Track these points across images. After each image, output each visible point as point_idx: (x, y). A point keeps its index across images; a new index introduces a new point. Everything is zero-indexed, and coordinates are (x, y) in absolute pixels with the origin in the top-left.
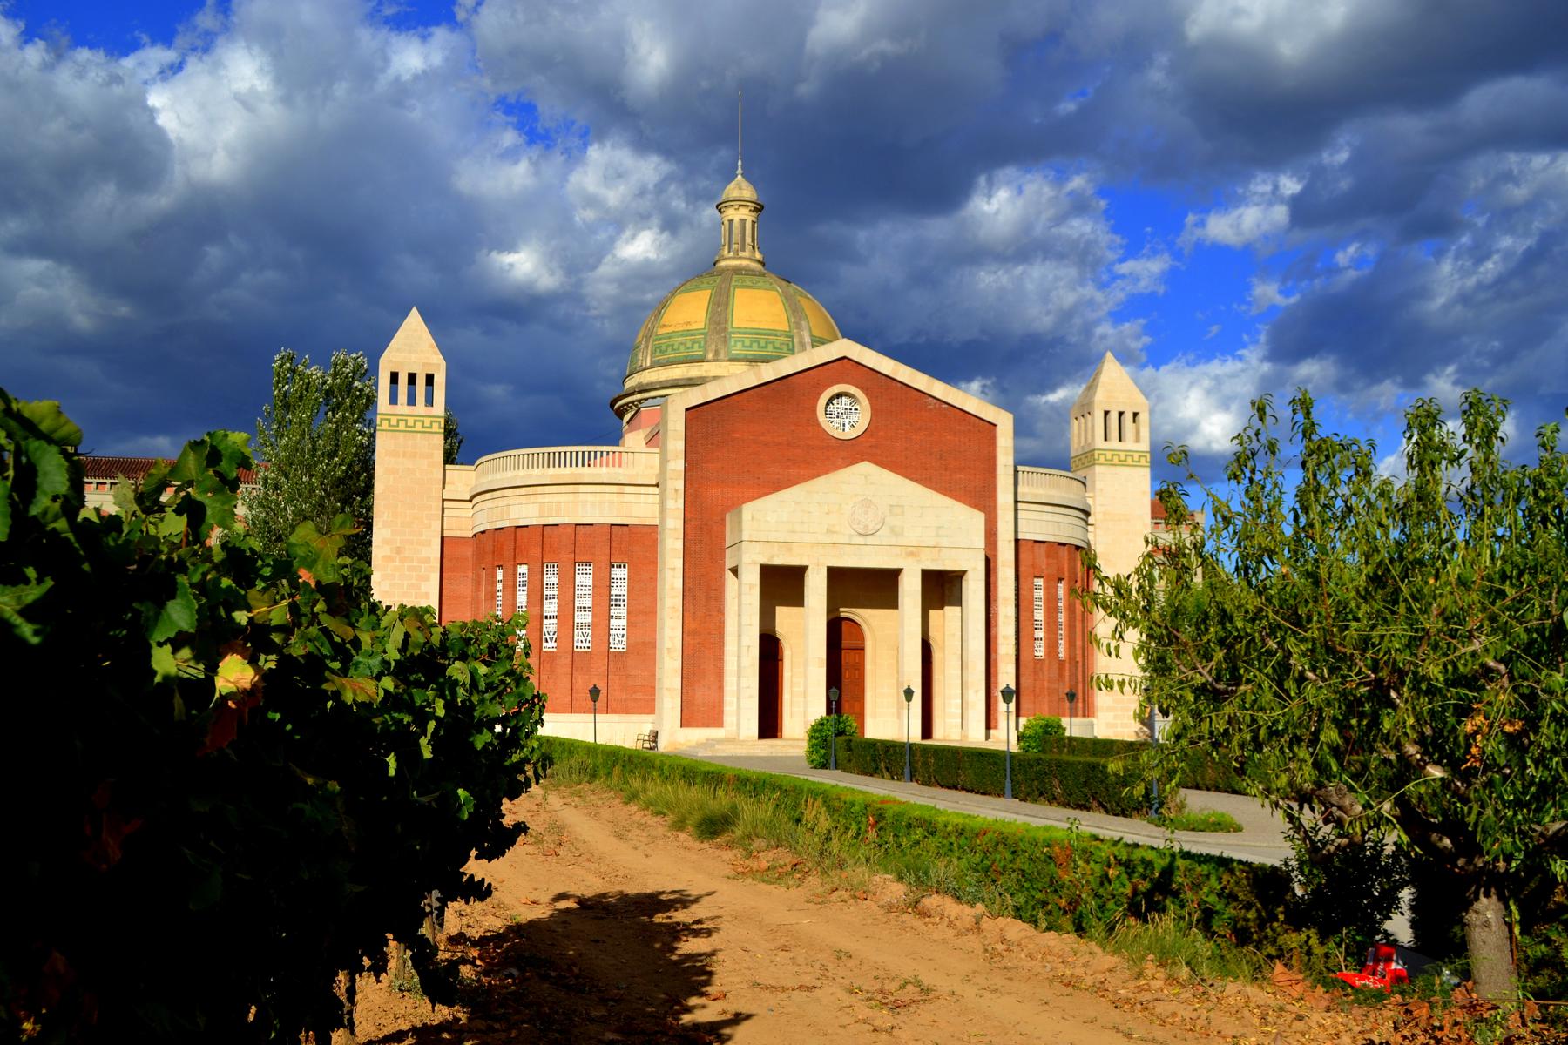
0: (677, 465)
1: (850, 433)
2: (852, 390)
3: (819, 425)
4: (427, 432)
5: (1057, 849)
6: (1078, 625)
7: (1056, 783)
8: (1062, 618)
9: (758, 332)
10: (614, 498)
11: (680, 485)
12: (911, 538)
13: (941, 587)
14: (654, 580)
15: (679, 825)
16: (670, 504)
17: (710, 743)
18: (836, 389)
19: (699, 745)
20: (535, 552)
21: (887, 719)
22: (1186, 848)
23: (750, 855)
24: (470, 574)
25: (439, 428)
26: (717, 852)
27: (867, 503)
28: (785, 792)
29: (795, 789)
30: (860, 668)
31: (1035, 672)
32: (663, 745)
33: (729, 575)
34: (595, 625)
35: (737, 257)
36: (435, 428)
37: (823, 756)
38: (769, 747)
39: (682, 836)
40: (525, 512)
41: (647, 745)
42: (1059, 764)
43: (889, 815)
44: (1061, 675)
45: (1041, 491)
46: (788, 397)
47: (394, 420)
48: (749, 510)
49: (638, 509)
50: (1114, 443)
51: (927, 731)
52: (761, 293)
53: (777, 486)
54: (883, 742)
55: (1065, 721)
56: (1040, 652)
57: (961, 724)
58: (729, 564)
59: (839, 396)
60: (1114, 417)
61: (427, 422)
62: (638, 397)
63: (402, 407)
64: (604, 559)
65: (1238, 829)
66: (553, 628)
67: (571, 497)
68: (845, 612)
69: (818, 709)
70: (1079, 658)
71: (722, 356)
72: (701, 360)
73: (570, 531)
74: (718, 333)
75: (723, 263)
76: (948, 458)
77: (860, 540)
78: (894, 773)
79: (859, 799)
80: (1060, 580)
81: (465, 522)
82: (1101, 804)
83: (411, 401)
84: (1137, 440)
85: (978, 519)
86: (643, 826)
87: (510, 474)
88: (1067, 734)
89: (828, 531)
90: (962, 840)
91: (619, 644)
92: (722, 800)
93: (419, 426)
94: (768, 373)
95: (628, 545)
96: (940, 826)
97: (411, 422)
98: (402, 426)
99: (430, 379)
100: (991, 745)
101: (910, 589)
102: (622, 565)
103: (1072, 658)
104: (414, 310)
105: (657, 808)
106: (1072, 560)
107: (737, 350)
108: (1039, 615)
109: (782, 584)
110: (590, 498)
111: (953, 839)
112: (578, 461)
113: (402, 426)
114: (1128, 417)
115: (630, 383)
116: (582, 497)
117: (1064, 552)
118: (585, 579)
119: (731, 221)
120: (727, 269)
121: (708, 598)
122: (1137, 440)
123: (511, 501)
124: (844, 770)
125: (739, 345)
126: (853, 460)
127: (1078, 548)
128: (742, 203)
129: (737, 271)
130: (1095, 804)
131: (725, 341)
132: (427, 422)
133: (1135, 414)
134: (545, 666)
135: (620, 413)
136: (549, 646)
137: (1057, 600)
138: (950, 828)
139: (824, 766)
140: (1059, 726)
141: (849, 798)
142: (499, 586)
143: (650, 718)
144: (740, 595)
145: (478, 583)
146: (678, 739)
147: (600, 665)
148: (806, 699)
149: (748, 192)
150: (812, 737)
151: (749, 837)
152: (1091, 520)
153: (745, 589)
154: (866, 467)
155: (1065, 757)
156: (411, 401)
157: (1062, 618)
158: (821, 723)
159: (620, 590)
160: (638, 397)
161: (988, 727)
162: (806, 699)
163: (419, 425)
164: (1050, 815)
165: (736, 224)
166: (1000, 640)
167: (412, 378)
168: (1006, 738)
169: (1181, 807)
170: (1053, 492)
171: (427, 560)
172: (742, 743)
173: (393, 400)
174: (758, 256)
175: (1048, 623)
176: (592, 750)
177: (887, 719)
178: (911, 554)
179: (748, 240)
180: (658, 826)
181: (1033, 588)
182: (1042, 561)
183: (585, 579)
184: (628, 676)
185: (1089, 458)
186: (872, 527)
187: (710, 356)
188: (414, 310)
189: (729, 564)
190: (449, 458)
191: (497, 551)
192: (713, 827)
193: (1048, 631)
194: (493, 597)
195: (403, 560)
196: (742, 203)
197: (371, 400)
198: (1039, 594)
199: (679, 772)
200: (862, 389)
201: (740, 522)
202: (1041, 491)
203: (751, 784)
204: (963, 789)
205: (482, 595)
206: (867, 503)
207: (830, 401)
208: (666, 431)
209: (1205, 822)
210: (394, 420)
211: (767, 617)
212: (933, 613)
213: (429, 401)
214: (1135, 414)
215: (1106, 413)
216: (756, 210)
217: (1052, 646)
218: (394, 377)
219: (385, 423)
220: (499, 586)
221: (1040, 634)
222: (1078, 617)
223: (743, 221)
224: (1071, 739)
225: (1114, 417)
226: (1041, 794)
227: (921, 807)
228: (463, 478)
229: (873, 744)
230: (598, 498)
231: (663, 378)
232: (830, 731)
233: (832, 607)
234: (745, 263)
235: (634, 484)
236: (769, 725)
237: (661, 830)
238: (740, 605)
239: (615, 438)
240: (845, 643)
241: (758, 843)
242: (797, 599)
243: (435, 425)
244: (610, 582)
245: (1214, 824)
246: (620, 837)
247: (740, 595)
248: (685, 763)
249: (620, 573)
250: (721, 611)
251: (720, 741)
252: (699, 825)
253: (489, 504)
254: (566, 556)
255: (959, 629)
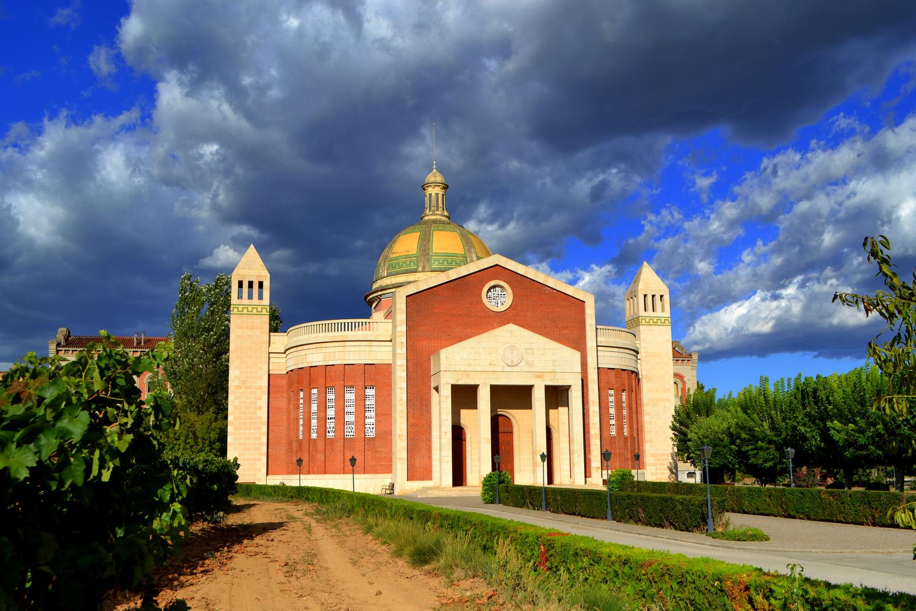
0: (402, 328)
1: (501, 308)
2: (502, 283)
3: (483, 304)
4: (259, 314)
5: (729, 583)
6: (634, 416)
7: (640, 510)
8: (625, 412)
9: (447, 255)
10: (367, 349)
11: (404, 340)
12: (538, 367)
13: (557, 396)
14: (390, 395)
15: (398, 554)
16: (399, 351)
17: (425, 490)
18: (492, 283)
19: (418, 491)
20: (322, 381)
21: (527, 473)
22: (806, 574)
23: (452, 584)
24: (285, 395)
25: (266, 312)
26: (427, 579)
27: (512, 348)
28: (475, 526)
29: (481, 523)
30: (510, 444)
31: (611, 444)
32: (397, 491)
33: (434, 391)
34: (356, 423)
35: (434, 214)
36: (264, 312)
37: (492, 496)
38: (458, 491)
39: (400, 562)
40: (315, 358)
41: (388, 492)
42: (642, 499)
43: (558, 545)
44: (626, 445)
45: (611, 340)
46: (466, 287)
47: (240, 308)
48: (444, 353)
49: (380, 355)
50: (650, 313)
51: (550, 480)
52: (448, 233)
53: (460, 339)
54: (528, 487)
55: (634, 472)
56: (613, 433)
57: (570, 476)
58: (433, 385)
59: (494, 287)
60: (649, 298)
61: (260, 308)
62: (380, 293)
63: (245, 301)
64: (361, 384)
65: (767, 539)
66: (332, 425)
67: (341, 349)
68: (501, 412)
69: (487, 469)
70: (635, 436)
71: (427, 269)
72: (415, 271)
73: (341, 368)
74: (424, 256)
75: (426, 218)
76: (556, 318)
77: (509, 369)
78: (536, 506)
79: (531, 531)
80: (624, 390)
81: (281, 365)
82: (671, 524)
83: (250, 297)
84: (663, 311)
85: (577, 355)
86: (374, 553)
87: (306, 337)
88: (635, 479)
89: (490, 364)
90: (626, 569)
91: (371, 433)
92: (429, 535)
93: (255, 311)
94: (453, 275)
95: (375, 375)
96: (605, 556)
97: (250, 309)
98: (245, 311)
99: (261, 285)
100: (588, 487)
101: (539, 397)
102: (372, 387)
103: (631, 435)
104: (252, 245)
105: (385, 538)
106: (630, 379)
107: (435, 265)
108: (612, 411)
109: (464, 396)
110: (352, 349)
111: (617, 567)
112: (345, 328)
113: (245, 311)
114: (658, 298)
115: (375, 286)
116: (348, 349)
117: (625, 374)
118: (350, 396)
119: (430, 195)
120: (429, 221)
121: (422, 405)
122: (663, 311)
123: (308, 352)
124: (505, 504)
125: (437, 263)
126: (503, 323)
127: (633, 372)
128: (436, 184)
129: (435, 222)
130: (667, 524)
131: (428, 260)
132: (260, 308)
133: (662, 296)
134: (328, 447)
135: (370, 303)
136: (331, 435)
137: (622, 402)
138: (613, 558)
139: (492, 502)
140: (631, 475)
141: (523, 531)
142: (301, 401)
143: (389, 475)
144: (440, 402)
145: (289, 400)
146: (406, 487)
147: (360, 446)
148: (479, 464)
149: (439, 179)
150: (484, 485)
151: (451, 567)
152: (639, 357)
153: (443, 399)
154: (511, 327)
155: (645, 494)
156: (250, 297)
157: (625, 412)
158: (490, 476)
159: (370, 402)
160: (380, 293)
161: (586, 477)
162: (479, 464)
163: (255, 311)
164: (641, 532)
165: (433, 195)
166: (591, 426)
167: (251, 284)
168: (597, 482)
169: (727, 525)
170: (617, 340)
171: (261, 387)
172: (443, 489)
173: (240, 296)
174: (446, 213)
175: (617, 415)
176: (351, 496)
177: (527, 473)
178: (539, 377)
179: (440, 205)
180: (384, 552)
181: (608, 395)
182: (613, 380)
183: (350, 396)
184: (376, 451)
185: (635, 322)
186: (515, 361)
187: (420, 269)
188: (252, 245)
189: (433, 385)
190: (273, 329)
191: (300, 381)
192: (423, 556)
193: (617, 420)
194: (298, 408)
195: (246, 388)
196: (436, 184)
197: (228, 294)
198: (612, 399)
199: (401, 511)
200: (507, 283)
201: (439, 360)
202: (611, 340)
203: (452, 522)
204: (579, 515)
205: (292, 407)
206: (512, 348)
207: (489, 290)
208: (395, 309)
209: (744, 534)
210: (240, 308)
211: (456, 415)
212: (551, 411)
213: (261, 297)
214: (662, 296)
215: (645, 296)
216: (444, 188)
217: (620, 429)
218: (240, 284)
219: (236, 310)
220: (301, 401)
221: (613, 422)
222: (634, 411)
223: (437, 194)
224: (638, 482)
225: (649, 298)
226: (631, 518)
227: (583, 538)
228: (280, 340)
229: (521, 488)
230: (357, 349)
231: (394, 282)
232: (495, 481)
233: (493, 409)
234: (439, 217)
235: (377, 340)
236: (459, 478)
237: (386, 557)
238: (440, 408)
239: (368, 315)
240: (501, 430)
241: (458, 573)
242: (473, 405)
243: (264, 311)
244: (365, 397)
245: (751, 536)
246: (354, 563)
247: (440, 402)
248: (405, 504)
249: (370, 392)
250: (429, 412)
251: (430, 488)
252: (412, 555)
253: (295, 354)
254: (339, 383)
255: (568, 420)
